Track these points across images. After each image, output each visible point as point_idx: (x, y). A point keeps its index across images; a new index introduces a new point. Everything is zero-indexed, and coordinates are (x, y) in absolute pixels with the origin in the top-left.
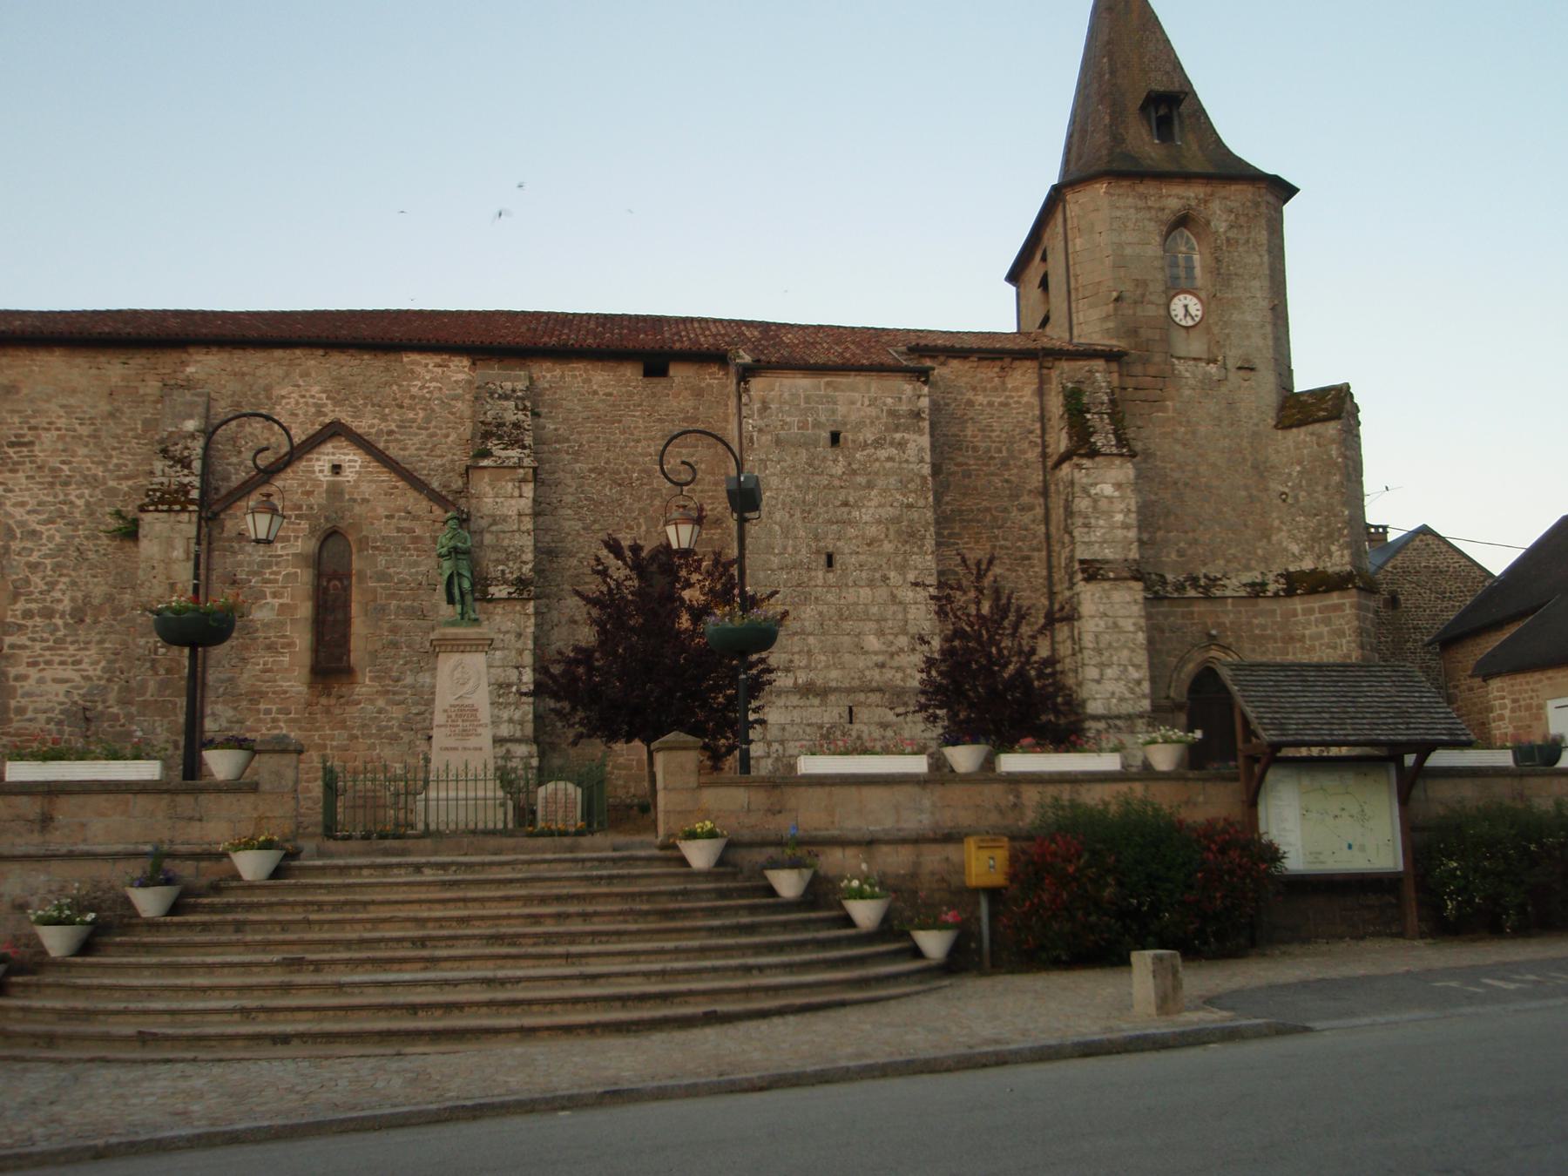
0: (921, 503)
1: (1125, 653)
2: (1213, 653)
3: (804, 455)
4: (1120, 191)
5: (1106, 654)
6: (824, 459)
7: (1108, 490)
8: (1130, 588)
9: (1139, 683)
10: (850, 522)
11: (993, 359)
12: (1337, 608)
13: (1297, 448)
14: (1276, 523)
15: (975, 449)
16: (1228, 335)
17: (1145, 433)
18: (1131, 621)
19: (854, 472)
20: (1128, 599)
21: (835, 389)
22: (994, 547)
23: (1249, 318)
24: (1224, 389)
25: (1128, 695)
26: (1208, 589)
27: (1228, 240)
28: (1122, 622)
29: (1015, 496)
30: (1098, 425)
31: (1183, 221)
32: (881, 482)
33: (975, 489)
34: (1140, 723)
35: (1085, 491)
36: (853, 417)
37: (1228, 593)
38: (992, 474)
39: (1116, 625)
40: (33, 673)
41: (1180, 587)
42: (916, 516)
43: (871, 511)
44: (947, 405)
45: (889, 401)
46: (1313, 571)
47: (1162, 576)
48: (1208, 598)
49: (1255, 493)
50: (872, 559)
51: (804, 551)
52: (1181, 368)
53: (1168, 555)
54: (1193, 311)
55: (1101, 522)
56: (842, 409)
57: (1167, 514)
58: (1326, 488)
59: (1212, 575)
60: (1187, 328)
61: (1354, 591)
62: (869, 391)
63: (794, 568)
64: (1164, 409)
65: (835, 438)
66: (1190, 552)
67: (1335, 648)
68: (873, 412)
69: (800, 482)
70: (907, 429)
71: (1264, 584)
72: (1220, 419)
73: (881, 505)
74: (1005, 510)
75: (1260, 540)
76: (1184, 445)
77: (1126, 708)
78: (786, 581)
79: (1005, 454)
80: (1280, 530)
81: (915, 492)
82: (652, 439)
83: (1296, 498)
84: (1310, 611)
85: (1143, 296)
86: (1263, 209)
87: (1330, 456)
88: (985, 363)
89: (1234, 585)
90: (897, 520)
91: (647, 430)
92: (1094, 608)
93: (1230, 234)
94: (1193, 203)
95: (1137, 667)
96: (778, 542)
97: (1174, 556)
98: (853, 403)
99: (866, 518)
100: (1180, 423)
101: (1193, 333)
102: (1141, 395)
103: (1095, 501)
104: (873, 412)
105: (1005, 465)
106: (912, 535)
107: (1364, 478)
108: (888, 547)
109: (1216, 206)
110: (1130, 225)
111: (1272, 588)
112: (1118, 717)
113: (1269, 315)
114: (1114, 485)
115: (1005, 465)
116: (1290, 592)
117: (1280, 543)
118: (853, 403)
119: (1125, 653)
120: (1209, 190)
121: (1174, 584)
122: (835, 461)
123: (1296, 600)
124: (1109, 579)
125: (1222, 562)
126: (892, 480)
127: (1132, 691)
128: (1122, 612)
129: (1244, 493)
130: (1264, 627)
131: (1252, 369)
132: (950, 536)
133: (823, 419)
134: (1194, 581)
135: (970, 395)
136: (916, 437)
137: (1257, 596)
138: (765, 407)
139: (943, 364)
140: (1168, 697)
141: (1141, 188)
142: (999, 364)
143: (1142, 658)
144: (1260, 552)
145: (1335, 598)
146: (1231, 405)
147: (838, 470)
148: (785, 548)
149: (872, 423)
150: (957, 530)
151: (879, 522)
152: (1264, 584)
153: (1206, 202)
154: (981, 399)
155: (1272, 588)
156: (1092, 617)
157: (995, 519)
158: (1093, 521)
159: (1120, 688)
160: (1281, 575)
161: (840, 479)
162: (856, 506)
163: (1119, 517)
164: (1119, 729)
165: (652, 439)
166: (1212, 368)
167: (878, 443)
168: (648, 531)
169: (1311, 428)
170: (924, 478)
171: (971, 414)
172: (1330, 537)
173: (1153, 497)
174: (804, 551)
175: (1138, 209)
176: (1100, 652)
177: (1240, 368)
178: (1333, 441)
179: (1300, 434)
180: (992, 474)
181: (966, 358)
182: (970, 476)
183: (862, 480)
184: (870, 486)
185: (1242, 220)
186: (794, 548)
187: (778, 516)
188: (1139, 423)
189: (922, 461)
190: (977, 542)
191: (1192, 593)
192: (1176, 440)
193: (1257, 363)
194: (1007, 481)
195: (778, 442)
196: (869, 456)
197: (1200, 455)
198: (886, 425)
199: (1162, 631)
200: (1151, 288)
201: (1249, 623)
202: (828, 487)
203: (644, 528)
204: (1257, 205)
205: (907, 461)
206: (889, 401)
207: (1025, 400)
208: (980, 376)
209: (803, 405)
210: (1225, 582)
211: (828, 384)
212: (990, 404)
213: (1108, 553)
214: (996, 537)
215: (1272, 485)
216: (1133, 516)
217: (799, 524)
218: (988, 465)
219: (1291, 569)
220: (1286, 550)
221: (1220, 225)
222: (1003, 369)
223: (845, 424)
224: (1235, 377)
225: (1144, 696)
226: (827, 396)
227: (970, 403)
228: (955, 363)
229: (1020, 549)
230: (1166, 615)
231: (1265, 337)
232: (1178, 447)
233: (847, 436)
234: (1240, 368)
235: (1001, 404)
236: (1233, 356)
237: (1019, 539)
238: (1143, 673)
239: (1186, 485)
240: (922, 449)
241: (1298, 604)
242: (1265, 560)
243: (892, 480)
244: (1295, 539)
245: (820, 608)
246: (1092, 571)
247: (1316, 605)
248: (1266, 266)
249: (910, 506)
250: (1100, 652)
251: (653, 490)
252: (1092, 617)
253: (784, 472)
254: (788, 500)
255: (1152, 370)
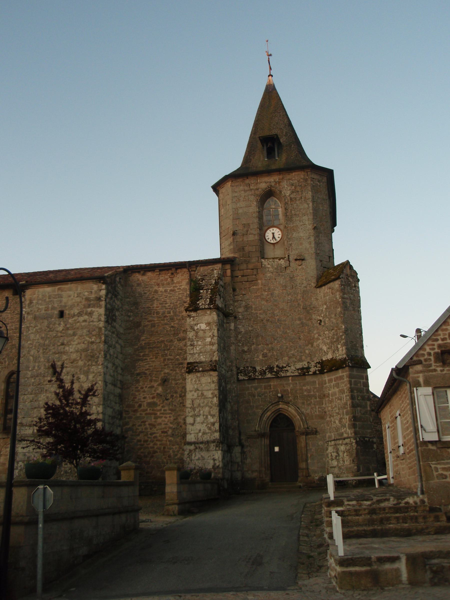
0: (98, 341)
1: (207, 409)
2: (281, 406)
3: (46, 323)
4: (236, 184)
5: (197, 410)
6: (55, 324)
7: (203, 326)
8: (211, 375)
9: (213, 424)
10: (64, 353)
11: (167, 270)
12: (341, 378)
13: (324, 297)
14: (316, 336)
15: (158, 313)
16: (291, 245)
17: (246, 297)
18: (210, 392)
19: (68, 329)
20: (209, 381)
21: (62, 291)
22: (165, 360)
23: (302, 235)
24: (288, 271)
25: (207, 431)
26: (277, 373)
27: (291, 199)
28: (205, 393)
29: (176, 334)
30: (204, 295)
31: (269, 194)
32: (79, 332)
33: (157, 332)
34: (212, 446)
35: (192, 328)
36: (70, 303)
37: (288, 374)
38: (166, 324)
39: (202, 394)
40: (139, 428)
41: (263, 373)
42: (95, 347)
43: (74, 347)
44: (145, 293)
45: (86, 293)
46: (332, 359)
47: (254, 368)
48: (278, 377)
49: (304, 321)
50: (73, 370)
51: (42, 368)
52: (266, 263)
53: (258, 357)
54: (276, 236)
55: (200, 343)
56: (64, 300)
57: (257, 336)
58: (335, 316)
59: (281, 366)
60: (274, 244)
61: (347, 368)
62: (77, 290)
63: (37, 376)
64: (257, 285)
65: (62, 314)
66: (269, 355)
67: (341, 400)
68: (78, 299)
69: (43, 335)
70: (94, 306)
71: (308, 368)
72: (286, 286)
73: (79, 343)
74: (171, 341)
75: (307, 345)
76: (267, 301)
77: (206, 438)
78: (33, 383)
79: (172, 314)
80: (318, 339)
81: (95, 335)
82: (14, 322)
83: (325, 322)
84: (330, 381)
85: (247, 231)
86: (309, 182)
87: (336, 298)
88: (164, 272)
89: (292, 370)
90: (85, 350)
91: (12, 318)
92: (192, 386)
93: (292, 196)
94: (273, 184)
95: (213, 416)
96: (31, 364)
97: (261, 357)
98: (70, 296)
99: (71, 350)
100: (265, 291)
101: (276, 246)
102: (245, 279)
103: (197, 333)
104: (78, 299)
105: (172, 319)
106: (92, 357)
107: (362, 308)
108: (81, 363)
109: (284, 184)
110: (242, 199)
111: (312, 370)
112: (202, 443)
113: (312, 232)
114: (206, 324)
115: (172, 319)
116: (322, 372)
117: (318, 346)
118: (70, 296)
119: (207, 409)
120: (281, 177)
121: (260, 371)
122: (59, 324)
123: (326, 375)
124: (199, 371)
125: (286, 358)
126: (85, 331)
127: (210, 429)
128: (206, 388)
129: (298, 322)
130: (309, 391)
131: (303, 260)
132: (144, 355)
133: (56, 305)
134: (271, 369)
135: (156, 288)
136: (98, 309)
137: (304, 375)
138: (31, 302)
139: (143, 275)
140: (255, 431)
141: (247, 181)
142: (170, 271)
143: (215, 411)
144: (307, 352)
145: (340, 373)
146: (292, 278)
147: (60, 328)
148: (34, 367)
149: (78, 305)
150: (147, 353)
151: (77, 351)
152: (308, 368)
153: (279, 182)
154: (161, 289)
155: (312, 370)
156: (191, 391)
157: (166, 346)
158: (195, 343)
159: (204, 428)
160: (319, 363)
161: (61, 332)
162: (68, 344)
163: (208, 340)
164: (201, 449)
165: (14, 322)
166: (282, 262)
167: (80, 314)
168: (9, 364)
169: (329, 285)
170: (100, 329)
171: (156, 297)
172: (338, 341)
173: (250, 328)
174: (42, 368)
175: (245, 191)
176: (194, 409)
177: (296, 260)
178: (337, 291)
179: (325, 289)
180: (166, 324)
181: (154, 271)
182: (154, 326)
183: (70, 332)
184: (74, 334)
185: (298, 189)
186: (38, 366)
187: (32, 353)
188: (243, 293)
189: (100, 320)
190: (156, 358)
191: (269, 375)
192: (263, 299)
193: (306, 256)
194: (172, 327)
195: (35, 318)
196: (75, 320)
197: (275, 305)
198: (84, 305)
199: (254, 396)
200: (251, 227)
201: (301, 389)
202: (56, 337)
203: (7, 363)
204: (306, 180)
205: (93, 321)
206: (86, 293)
207: (183, 287)
208: (161, 278)
209: (47, 300)
210: (288, 368)
211: (59, 289)
212: (166, 291)
213: (202, 358)
214: (166, 355)
215: (314, 316)
216: (216, 338)
217: (41, 356)
218: (164, 320)
219: (324, 359)
220: (321, 349)
221: (287, 193)
222: (172, 274)
223: (65, 306)
224: (293, 264)
225: (216, 431)
226: (58, 295)
227: (156, 292)
228: (149, 274)
229: (178, 360)
230: (256, 388)
231: (310, 243)
232: (263, 302)
233: (66, 312)
234: (296, 260)
235: (171, 290)
236: (293, 255)
237: (177, 355)
238: (216, 419)
239: (268, 320)
240: (100, 315)
241: (326, 377)
242: (310, 355)
243: (85, 331)
244: (325, 344)
245: (48, 395)
246: (192, 368)
247: (333, 377)
248: (311, 208)
249: (92, 343)
250: (194, 409)
251: (13, 345)
252: (191, 391)
253: (37, 331)
254: (38, 344)
255: (251, 266)
